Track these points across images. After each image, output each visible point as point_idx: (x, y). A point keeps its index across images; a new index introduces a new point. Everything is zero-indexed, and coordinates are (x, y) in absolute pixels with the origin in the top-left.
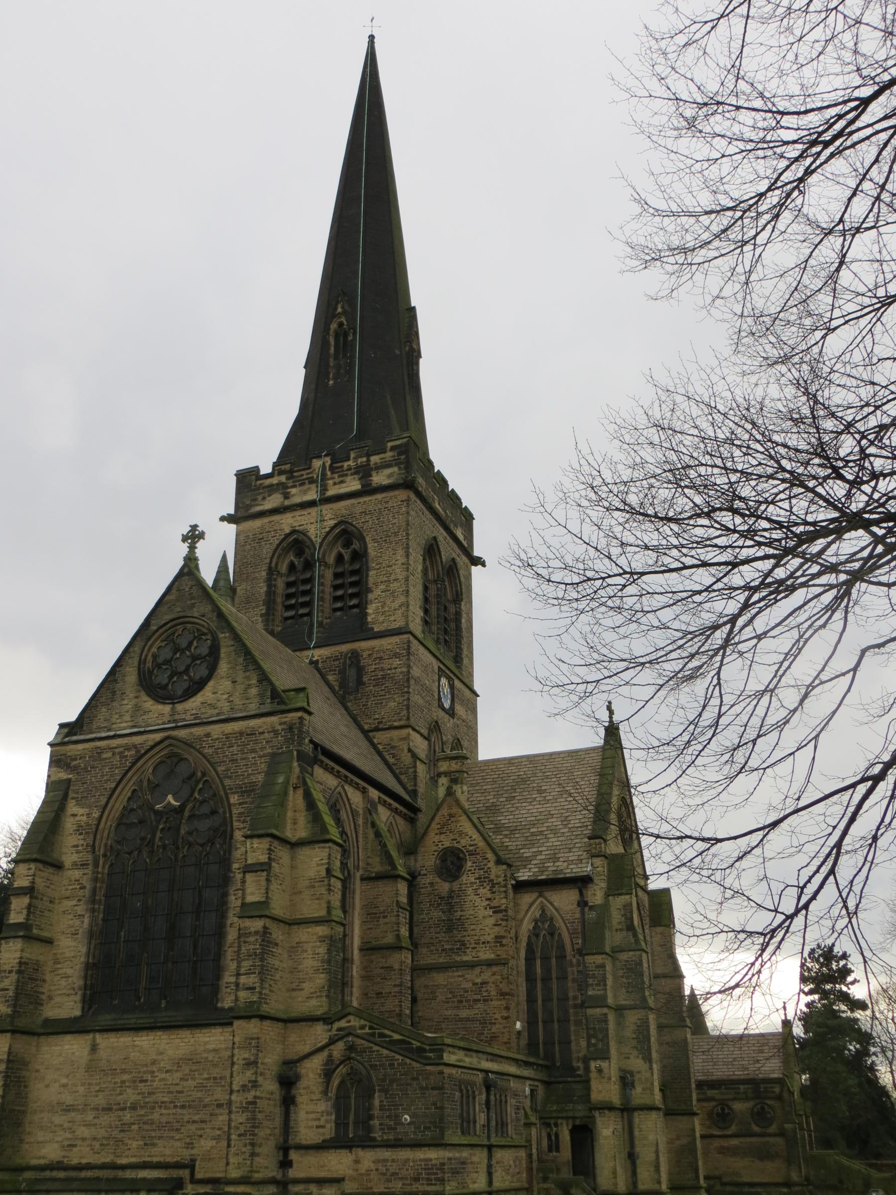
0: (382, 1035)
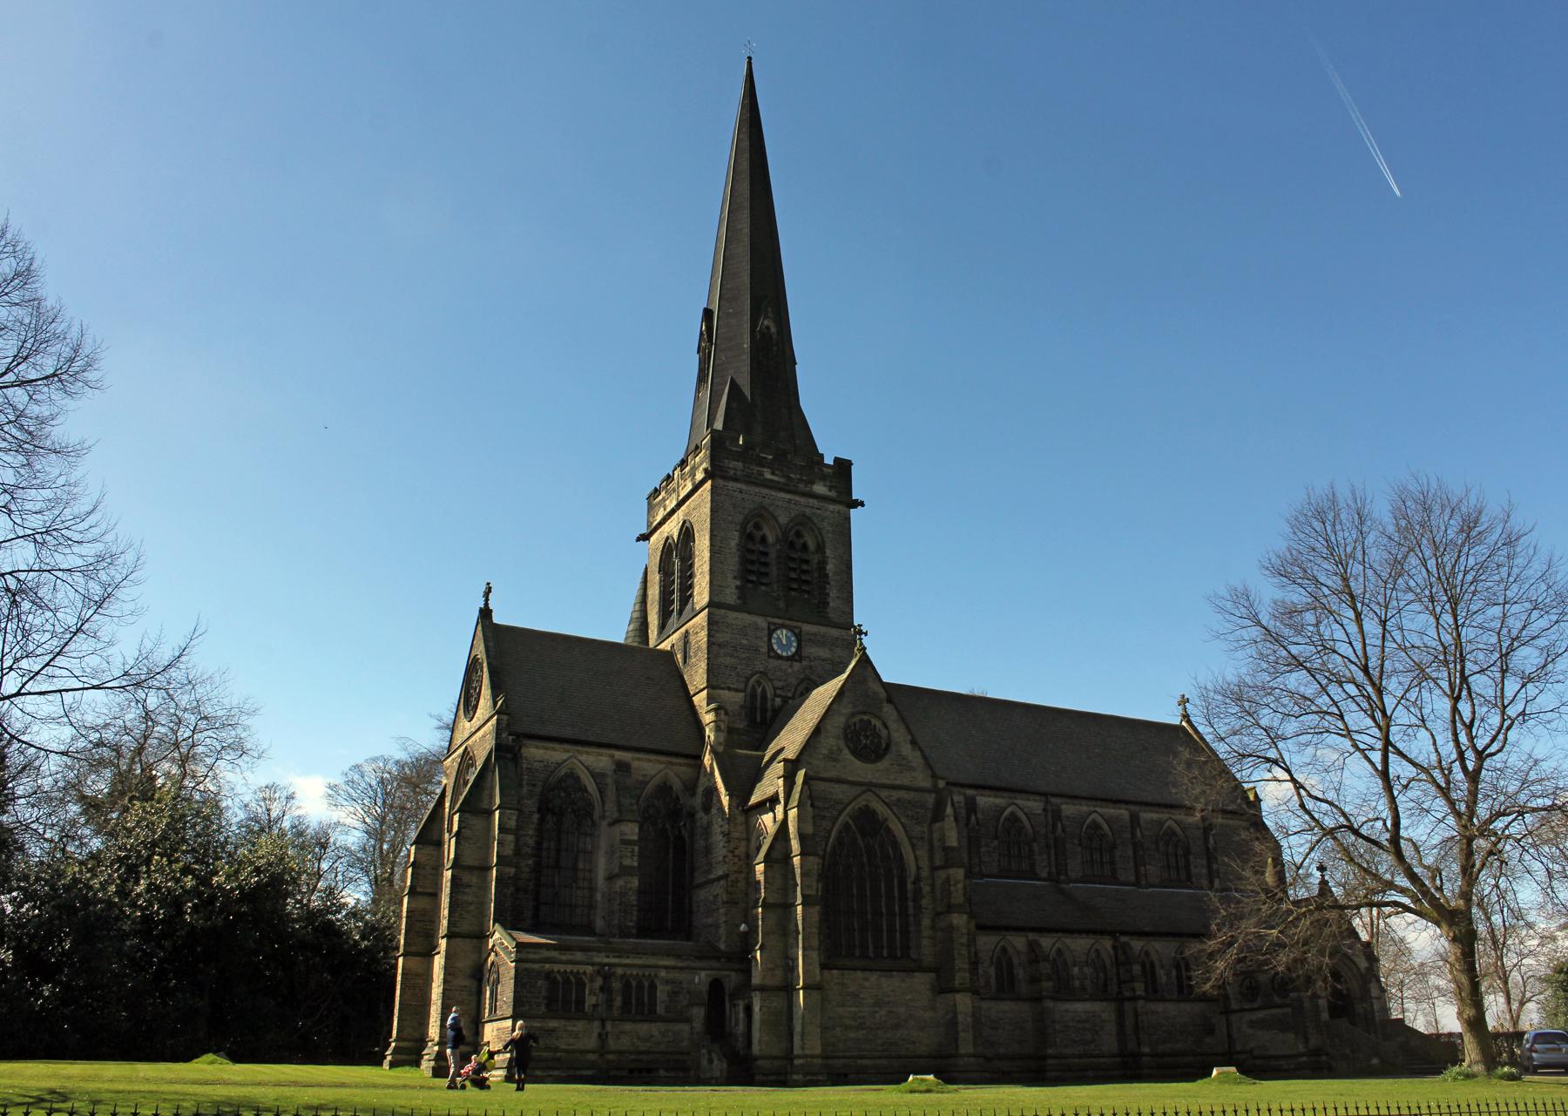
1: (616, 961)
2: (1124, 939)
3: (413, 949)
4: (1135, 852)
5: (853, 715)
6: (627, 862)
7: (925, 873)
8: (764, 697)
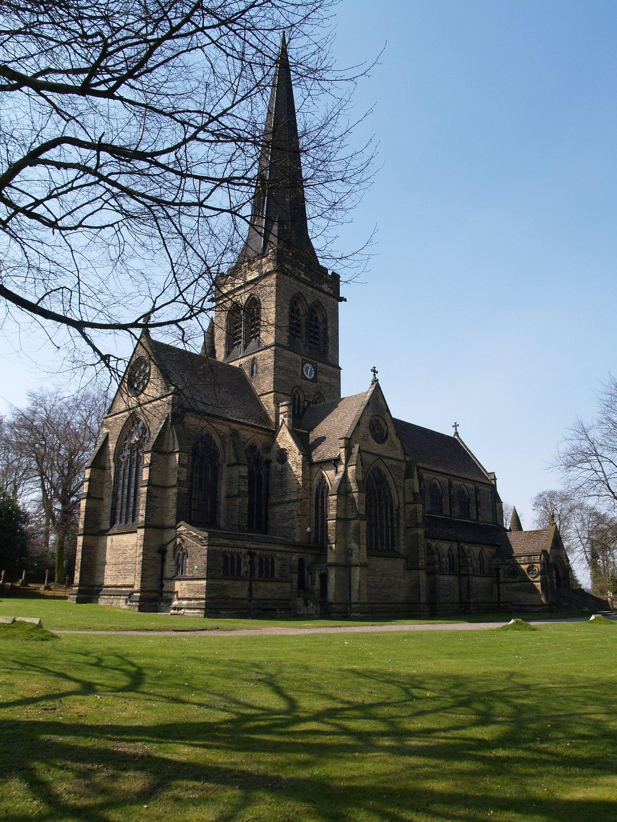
0: (191, 534)
1: (254, 546)
2: (462, 544)
3: (89, 531)
4: (450, 500)
5: (373, 416)
6: (242, 488)
7: (402, 506)
8: (299, 401)
